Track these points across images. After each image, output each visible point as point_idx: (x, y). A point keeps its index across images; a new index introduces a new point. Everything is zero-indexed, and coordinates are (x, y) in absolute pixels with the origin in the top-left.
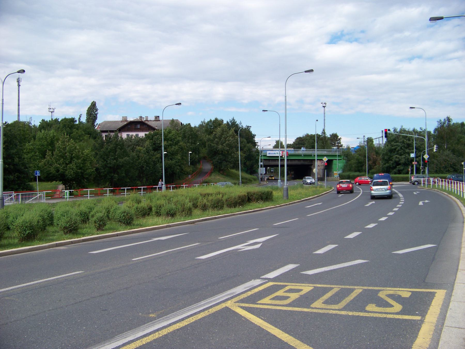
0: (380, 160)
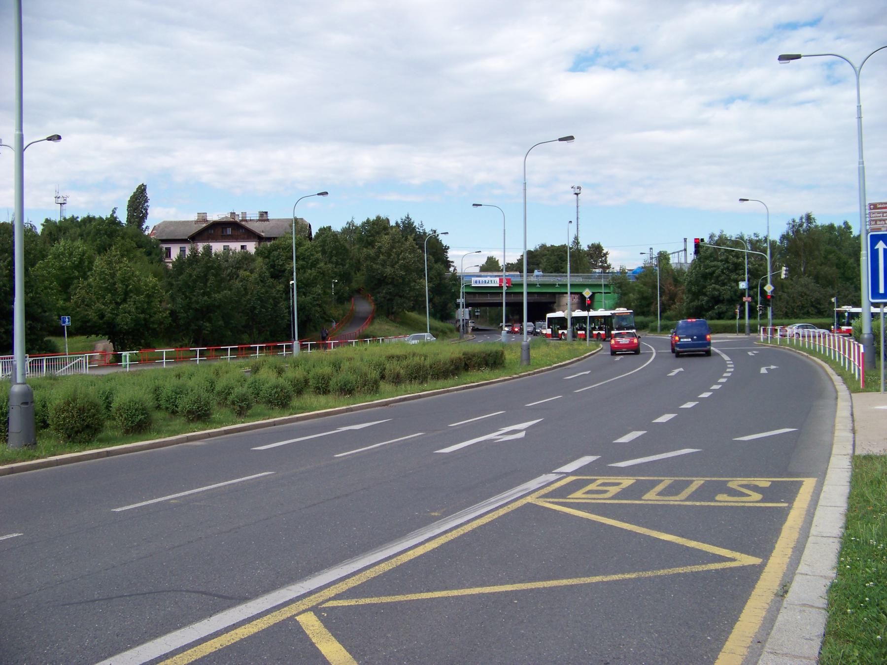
0: (683, 293)
